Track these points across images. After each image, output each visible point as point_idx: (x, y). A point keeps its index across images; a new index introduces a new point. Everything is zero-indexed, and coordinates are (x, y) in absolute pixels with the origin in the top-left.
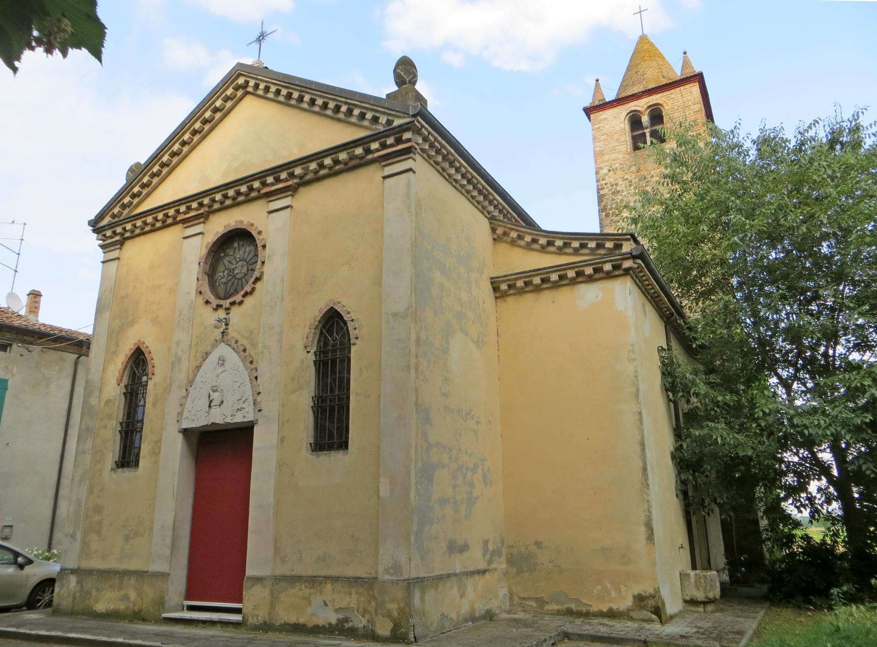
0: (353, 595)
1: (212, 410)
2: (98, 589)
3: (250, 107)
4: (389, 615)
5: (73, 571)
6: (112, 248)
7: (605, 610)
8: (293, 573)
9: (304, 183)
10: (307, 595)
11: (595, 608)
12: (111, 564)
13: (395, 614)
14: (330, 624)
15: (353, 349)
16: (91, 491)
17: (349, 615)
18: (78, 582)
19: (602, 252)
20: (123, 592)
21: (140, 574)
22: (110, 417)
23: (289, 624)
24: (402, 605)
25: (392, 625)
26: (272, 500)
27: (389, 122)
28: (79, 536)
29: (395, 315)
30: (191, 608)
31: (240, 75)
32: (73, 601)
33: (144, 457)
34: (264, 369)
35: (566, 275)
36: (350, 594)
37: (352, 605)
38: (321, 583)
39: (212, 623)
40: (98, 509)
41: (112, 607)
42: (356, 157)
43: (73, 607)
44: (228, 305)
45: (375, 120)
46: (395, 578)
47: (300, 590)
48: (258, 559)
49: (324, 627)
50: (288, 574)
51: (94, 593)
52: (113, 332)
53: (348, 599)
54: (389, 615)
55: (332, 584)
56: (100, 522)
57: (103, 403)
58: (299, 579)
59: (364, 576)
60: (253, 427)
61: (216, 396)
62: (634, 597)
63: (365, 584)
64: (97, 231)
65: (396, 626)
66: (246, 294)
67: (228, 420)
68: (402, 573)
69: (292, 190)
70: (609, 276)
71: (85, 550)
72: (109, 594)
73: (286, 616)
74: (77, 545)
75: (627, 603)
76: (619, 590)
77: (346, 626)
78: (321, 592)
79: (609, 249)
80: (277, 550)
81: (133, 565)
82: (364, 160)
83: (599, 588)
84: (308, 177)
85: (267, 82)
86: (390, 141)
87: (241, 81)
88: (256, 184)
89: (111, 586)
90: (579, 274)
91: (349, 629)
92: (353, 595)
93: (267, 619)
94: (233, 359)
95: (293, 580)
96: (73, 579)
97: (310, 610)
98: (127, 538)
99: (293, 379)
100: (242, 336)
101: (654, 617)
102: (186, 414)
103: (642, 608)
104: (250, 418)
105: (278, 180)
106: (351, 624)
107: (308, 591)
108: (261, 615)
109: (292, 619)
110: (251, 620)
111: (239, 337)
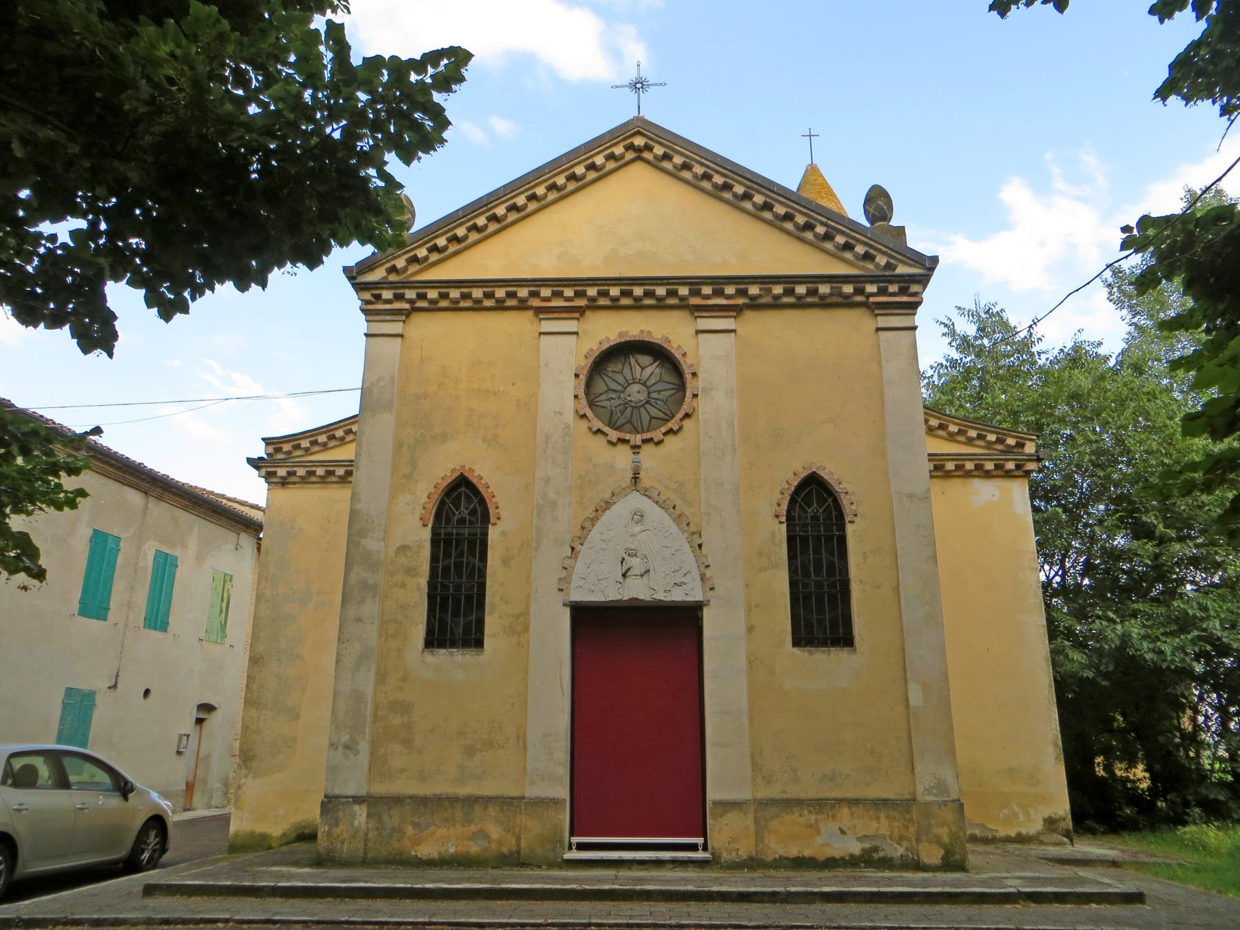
0: (883, 819)
1: (628, 580)
2: (416, 825)
3: (639, 178)
4: (938, 841)
5: (358, 800)
6: (388, 318)
7: (1013, 835)
8: (785, 796)
9: (755, 305)
10: (813, 821)
11: (1002, 832)
12: (440, 787)
13: (946, 840)
14: (852, 856)
15: (850, 529)
16: (381, 677)
17: (877, 843)
18: (369, 816)
19: (999, 447)
20: (473, 828)
21: (505, 802)
22: (411, 571)
23: (787, 858)
24: (954, 828)
25: (943, 852)
26: (744, 704)
27: (889, 266)
28: (364, 746)
29: (910, 496)
30: (581, 847)
31: (639, 133)
32: (366, 845)
33: (494, 635)
34: (711, 536)
35: (963, 466)
36: (878, 819)
37: (881, 832)
38: (833, 807)
39: (659, 863)
40: (404, 708)
41: (452, 850)
42: (841, 294)
43: (365, 853)
44: (639, 442)
45: (867, 257)
46: (940, 799)
47: (801, 815)
48: (725, 775)
49: (843, 859)
50: (778, 797)
51: (410, 830)
52: (401, 446)
53: (875, 824)
54: (938, 841)
55: (850, 808)
56: (409, 727)
57: (392, 550)
58: (799, 803)
59: (892, 797)
60: (701, 610)
61: (634, 562)
62: (1045, 820)
63: (903, 806)
64: (359, 287)
65: (948, 853)
66: (670, 432)
67: (661, 596)
68: (948, 793)
69: (735, 311)
70: (1008, 475)
71: (378, 765)
72: (442, 832)
73: (776, 848)
74: (363, 758)
75: (1036, 827)
76: (1027, 813)
77: (876, 856)
78: (834, 817)
79: (1009, 446)
80: (755, 766)
81: (489, 788)
82: (849, 301)
83: (1005, 811)
84: (763, 301)
85: (687, 157)
86: (893, 288)
87: (639, 141)
88: (684, 291)
89: (446, 820)
90: (979, 467)
91: (879, 859)
92: (883, 819)
93: (754, 854)
94: (654, 513)
95: (789, 804)
96: (361, 812)
97: (819, 840)
98: (470, 751)
99: (760, 554)
100: (666, 487)
101: (1065, 840)
102: (575, 581)
103: (1055, 831)
104: (696, 595)
105: (718, 293)
106: (881, 854)
107: (813, 817)
108: (744, 849)
109: (793, 852)
110: (725, 856)
111: (661, 489)
